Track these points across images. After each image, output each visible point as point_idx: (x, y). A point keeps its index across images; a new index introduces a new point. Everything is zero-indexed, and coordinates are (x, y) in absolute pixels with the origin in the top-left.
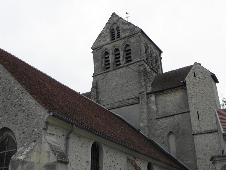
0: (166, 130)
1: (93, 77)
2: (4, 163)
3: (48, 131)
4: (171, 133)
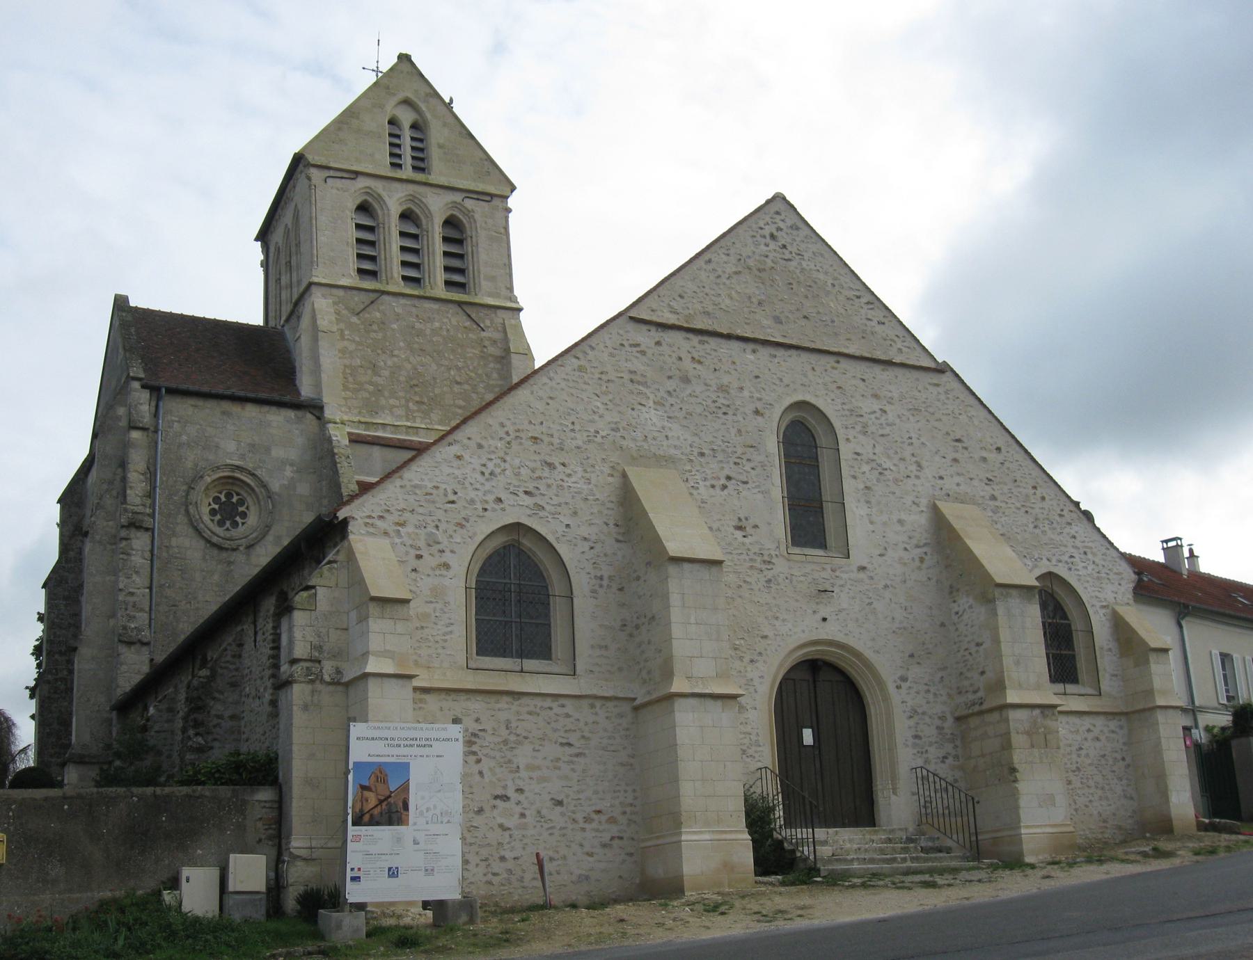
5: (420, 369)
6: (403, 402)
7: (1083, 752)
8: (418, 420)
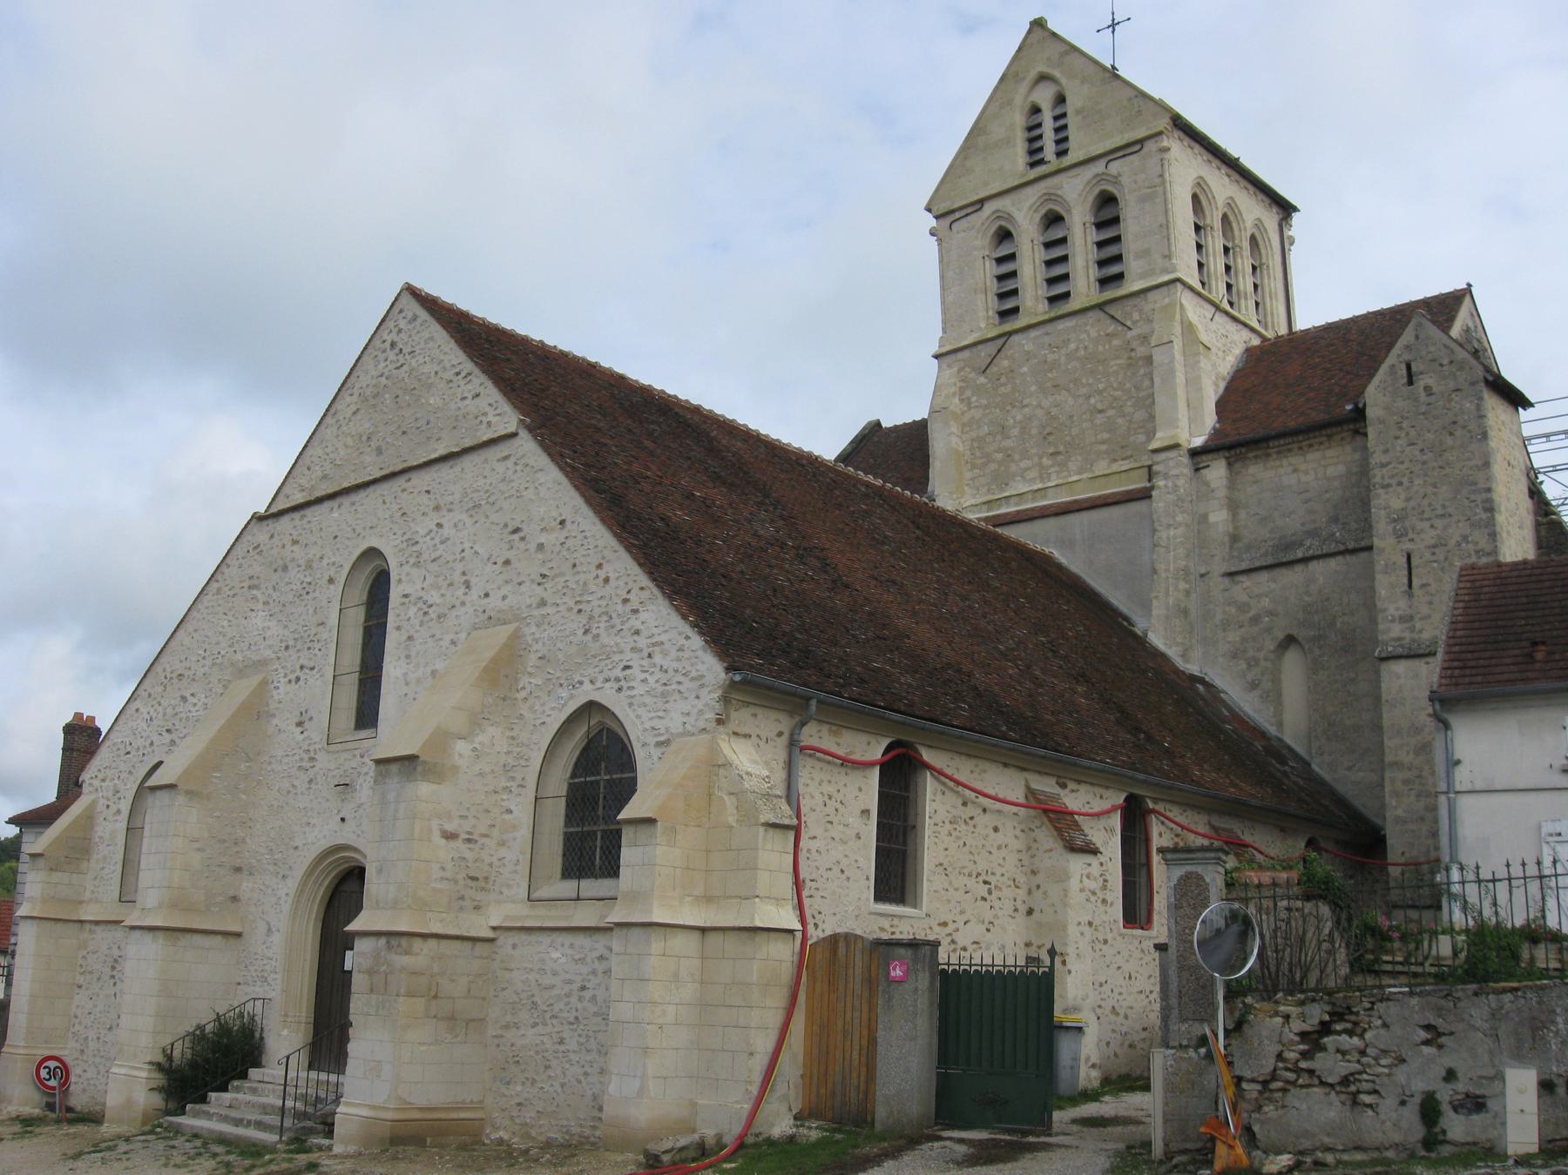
0: (1268, 630)
1: (936, 357)
2: (600, 812)
3: (733, 726)
4: (1290, 641)
5: (1054, 411)
6: (1036, 459)
7: (588, 994)
8: (1054, 476)
